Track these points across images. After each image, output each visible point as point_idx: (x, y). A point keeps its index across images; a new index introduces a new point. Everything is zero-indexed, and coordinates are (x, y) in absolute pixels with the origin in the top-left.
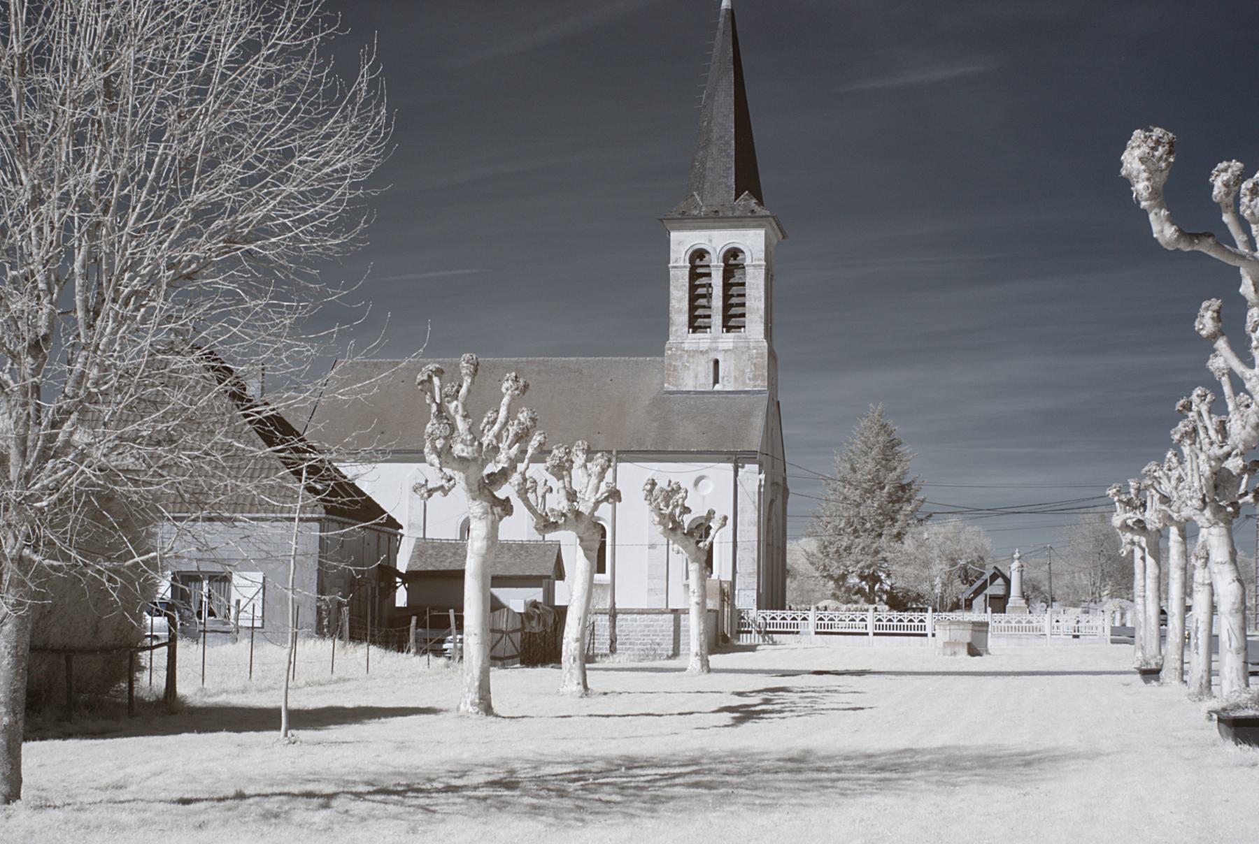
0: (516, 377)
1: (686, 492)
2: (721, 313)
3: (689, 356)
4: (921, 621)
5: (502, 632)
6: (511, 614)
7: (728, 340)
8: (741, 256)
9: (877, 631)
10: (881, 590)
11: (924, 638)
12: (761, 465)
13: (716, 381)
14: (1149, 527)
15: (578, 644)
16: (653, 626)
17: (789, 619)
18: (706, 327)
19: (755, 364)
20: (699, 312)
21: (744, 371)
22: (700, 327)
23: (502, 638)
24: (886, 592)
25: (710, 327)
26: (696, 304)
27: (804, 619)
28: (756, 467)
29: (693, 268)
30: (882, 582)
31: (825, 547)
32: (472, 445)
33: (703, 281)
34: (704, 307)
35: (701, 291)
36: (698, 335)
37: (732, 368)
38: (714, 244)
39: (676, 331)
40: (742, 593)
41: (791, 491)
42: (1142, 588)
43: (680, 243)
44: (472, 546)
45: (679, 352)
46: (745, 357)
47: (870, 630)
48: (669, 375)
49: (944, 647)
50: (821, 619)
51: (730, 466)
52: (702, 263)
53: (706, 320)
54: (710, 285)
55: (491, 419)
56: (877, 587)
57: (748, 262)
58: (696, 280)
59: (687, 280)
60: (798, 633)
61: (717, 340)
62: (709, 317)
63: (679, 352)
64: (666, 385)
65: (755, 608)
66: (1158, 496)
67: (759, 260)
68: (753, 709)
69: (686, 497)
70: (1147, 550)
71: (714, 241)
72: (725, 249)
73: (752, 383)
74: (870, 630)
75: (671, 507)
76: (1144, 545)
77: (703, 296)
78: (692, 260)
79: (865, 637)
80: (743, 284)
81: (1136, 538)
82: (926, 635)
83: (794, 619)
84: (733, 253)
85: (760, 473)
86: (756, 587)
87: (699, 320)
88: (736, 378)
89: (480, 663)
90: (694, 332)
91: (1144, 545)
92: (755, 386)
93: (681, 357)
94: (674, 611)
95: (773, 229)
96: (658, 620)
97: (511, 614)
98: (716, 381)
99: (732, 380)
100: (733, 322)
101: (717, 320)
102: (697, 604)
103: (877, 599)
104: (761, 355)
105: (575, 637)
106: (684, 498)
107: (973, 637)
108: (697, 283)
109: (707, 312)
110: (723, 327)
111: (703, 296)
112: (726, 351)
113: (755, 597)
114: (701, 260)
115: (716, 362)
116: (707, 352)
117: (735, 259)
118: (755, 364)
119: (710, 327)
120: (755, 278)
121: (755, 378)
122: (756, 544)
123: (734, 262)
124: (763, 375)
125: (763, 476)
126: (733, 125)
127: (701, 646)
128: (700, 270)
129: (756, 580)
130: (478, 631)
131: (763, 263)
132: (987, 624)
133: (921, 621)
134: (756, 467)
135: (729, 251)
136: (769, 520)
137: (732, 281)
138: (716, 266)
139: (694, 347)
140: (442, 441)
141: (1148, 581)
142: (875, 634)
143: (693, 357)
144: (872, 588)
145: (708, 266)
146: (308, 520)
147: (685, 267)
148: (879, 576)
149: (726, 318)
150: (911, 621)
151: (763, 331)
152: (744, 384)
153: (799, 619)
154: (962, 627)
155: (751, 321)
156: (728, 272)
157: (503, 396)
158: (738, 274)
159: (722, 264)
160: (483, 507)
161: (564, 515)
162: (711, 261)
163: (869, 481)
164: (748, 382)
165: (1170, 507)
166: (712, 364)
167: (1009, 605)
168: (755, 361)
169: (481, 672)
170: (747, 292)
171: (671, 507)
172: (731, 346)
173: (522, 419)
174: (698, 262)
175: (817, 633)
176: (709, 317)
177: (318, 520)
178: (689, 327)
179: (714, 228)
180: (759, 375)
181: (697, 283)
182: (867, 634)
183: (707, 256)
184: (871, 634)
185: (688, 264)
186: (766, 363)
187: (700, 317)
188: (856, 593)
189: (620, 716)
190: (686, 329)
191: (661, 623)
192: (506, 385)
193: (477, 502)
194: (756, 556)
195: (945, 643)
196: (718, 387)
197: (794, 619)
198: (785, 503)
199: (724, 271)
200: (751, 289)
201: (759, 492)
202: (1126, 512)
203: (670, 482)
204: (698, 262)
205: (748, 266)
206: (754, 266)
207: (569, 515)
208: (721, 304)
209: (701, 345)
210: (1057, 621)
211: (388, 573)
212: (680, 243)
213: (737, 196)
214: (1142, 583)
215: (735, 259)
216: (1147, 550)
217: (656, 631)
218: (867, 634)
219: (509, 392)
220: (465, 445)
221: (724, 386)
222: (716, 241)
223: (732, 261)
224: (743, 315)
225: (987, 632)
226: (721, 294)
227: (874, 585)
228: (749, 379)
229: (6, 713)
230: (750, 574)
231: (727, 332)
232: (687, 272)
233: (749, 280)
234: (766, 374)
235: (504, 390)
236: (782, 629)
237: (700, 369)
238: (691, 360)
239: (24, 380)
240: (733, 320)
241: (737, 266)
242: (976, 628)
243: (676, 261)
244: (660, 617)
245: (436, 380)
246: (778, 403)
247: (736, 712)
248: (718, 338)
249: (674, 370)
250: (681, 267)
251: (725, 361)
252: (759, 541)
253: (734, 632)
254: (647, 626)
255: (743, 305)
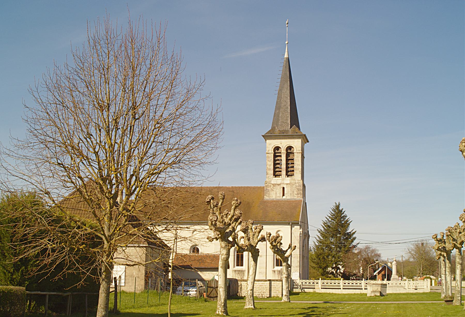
0: (237, 199)
1: (282, 237)
2: (285, 170)
3: (273, 186)
4: (360, 284)
5: (213, 288)
6: (216, 281)
7: (288, 180)
8: (292, 149)
9: (344, 287)
10: (340, 272)
11: (361, 290)
12: (300, 226)
13: (283, 195)
14: (447, 249)
15: (251, 291)
16: (262, 286)
17: (311, 283)
18: (279, 175)
19: (298, 189)
20: (277, 170)
21: (294, 191)
22: (277, 175)
23: (213, 290)
24: (341, 273)
25: (281, 175)
26: (276, 167)
27: (317, 283)
28: (299, 227)
29: (275, 153)
30: (340, 269)
31: (318, 256)
32: (222, 223)
33: (279, 158)
34: (278, 168)
35: (277, 162)
36: (276, 178)
37: (289, 190)
38: (282, 145)
39: (269, 177)
40: (294, 273)
41: (310, 236)
42: (444, 271)
43: (270, 144)
44: (221, 257)
45: (270, 185)
46: (294, 186)
47: (341, 287)
48: (266, 193)
49: (371, 293)
50: (323, 283)
51: (289, 227)
52: (278, 152)
53: (280, 173)
54: (281, 160)
55: (226, 213)
56: (338, 271)
57: (295, 151)
58: (276, 158)
59: (273, 158)
60: (314, 288)
61: (283, 180)
62: (281, 171)
63: (270, 185)
64: (265, 197)
65: (299, 279)
66: (452, 238)
67: (299, 150)
68: (309, 313)
69: (282, 239)
70: (446, 258)
71: (282, 144)
72: (287, 146)
73: (297, 196)
74: (341, 287)
75: (277, 243)
76: (445, 255)
77: (279, 164)
78: (274, 151)
79: (340, 290)
80: (293, 159)
81: (442, 253)
82: (362, 289)
83: (313, 283)
84: (290, 148)
85: (300, 229)
86: (299, 271)
87: (277, 173)
88: (291, 194)
89: (224, 297)
90: (275, 177)
91: (445, 255)
92: (298, 197)
93: (270, 186)
94: (270, 280)
95: (304, 139)
96: (264, 284)
97: (216, 281)
98: (283, 195)
99: (289, 195)
100: (289, 173)
101: (284, 172)
102: (286, 277)
103: (338, 276)
104: (300, 186)
105: (250, 289)
106: (281, 239)
107: (381, 289)
108: (276, 159)
109: (280, 170)
110: (286, 175)
111: (279, 164)
112: (287, 184)
113: (299, 275)
114: (278, 150)
115: (284, 188)
116: (280, 184)
117: (290, 150)
118: (298, 189)
119: (281, 175)
120: (297, 157)
121: (298, 194)
122: (299, 255)
123: (290, 151)
124: (301, 193)
125: (301, 230)
126: (289, 101)
127: (287, 292)
128: (277, 154)
129: (299, 269)
130: (223, 286)
131: (301, 151)
132: (386, 285)
133: (360, 284)
134: (299, 227)
135: (288, 147)
136: (303, 246)
137: (289, 158)
138: (283, 153)
139: (275, 183)
140: (214, 222)
141: (447, 269)
142: (343, 289)
143: (275, 186)
144: (336, 272)
145: (280, 153)
146: (142, 247)
147: (272, 153)
148: (339, 267)
149: (287, 172)
150: (352, 284)
151: (301, 177)
152: (294, 196)
153: (315, 283)
154: (377, 286)
155: (296, 173)
156: (288, 155)
157: (232, 205)
158: (291, 155)
159: (286, 152)
160: (225, 244)
161: (247, 246)
162: (281, 151)
163: (335, 231)
164: (295, 195)
165: (457, 242)
166: (282, 189)
167: (392, 278)
168: (298, 188)
169: (224, 301)
170: (295, 162)
171: (277, 243)
172: (289, 182)
173: (237, 214)
174: (276, 151)
175: (322, 288)
176: (281, 171)
177: (145, 247)
178: (274, 175)
179: (282, 139)
180: (299, 193)
181: (276, 159)
182: (340, 289)
183: (280, 149)
184: (342, 289)
185: (273, 152)
186: (302, 188)
187: (277, 171)
188: (330, 274)
189: (270, 316)
190: (272, 176)
191: (265, 284)
192: (233, 202)
193: (223, 242)
194: (299, 260)
195: (371, 292)
196: (284, 197)
197: (313, 283)
198: (308, 240)
199: (286, 155)
200: (296, 161)
201: (300, 236)
202: (439, 244)
203: (267, 232)
204: (276, 151)
205: (295, 153)
206: (297, 153)
207: (248, 246)
208: (285, 167)
209: (278, 182)
210: (410, 284)
211: (166, 265)
212: (270, 144)
213: (291, 127)
214: (444, 269)
215: (290, 150)
216: (446, 258)
217: (264, 287)
218: (340, 289)
219: (235, 204)
220: (220, 223)
221: (286, 197)
222: (283, 144)
223: (289, 151)
224: (293, 171)
225: (386, 287)
226: (285, 163)
227: (337, 270)
228: (296, 194)
229: (103, 311)
230: (297, 266)
231: (288, 177)
232: (272, 155)
233: (295, 158)
234: (302, 193)
235: (232, 204)
236: (309, 287)
237: (277, 191)
238: (274, 187)
239: (169, 213)
240: (289, 172)
241: (291, 153)
242: (383, 286)
243: (268, 151)
244: (265, 282)
245: (212, 201)
246: (306, 203)
247: (304, 314)
248: (284, 179)
249: (268, 191)
250: (270, 153)
251: (287, 188)
252: (300, 255)
253: (291, 288)
254: (260, 286)
255: (293, 167)
